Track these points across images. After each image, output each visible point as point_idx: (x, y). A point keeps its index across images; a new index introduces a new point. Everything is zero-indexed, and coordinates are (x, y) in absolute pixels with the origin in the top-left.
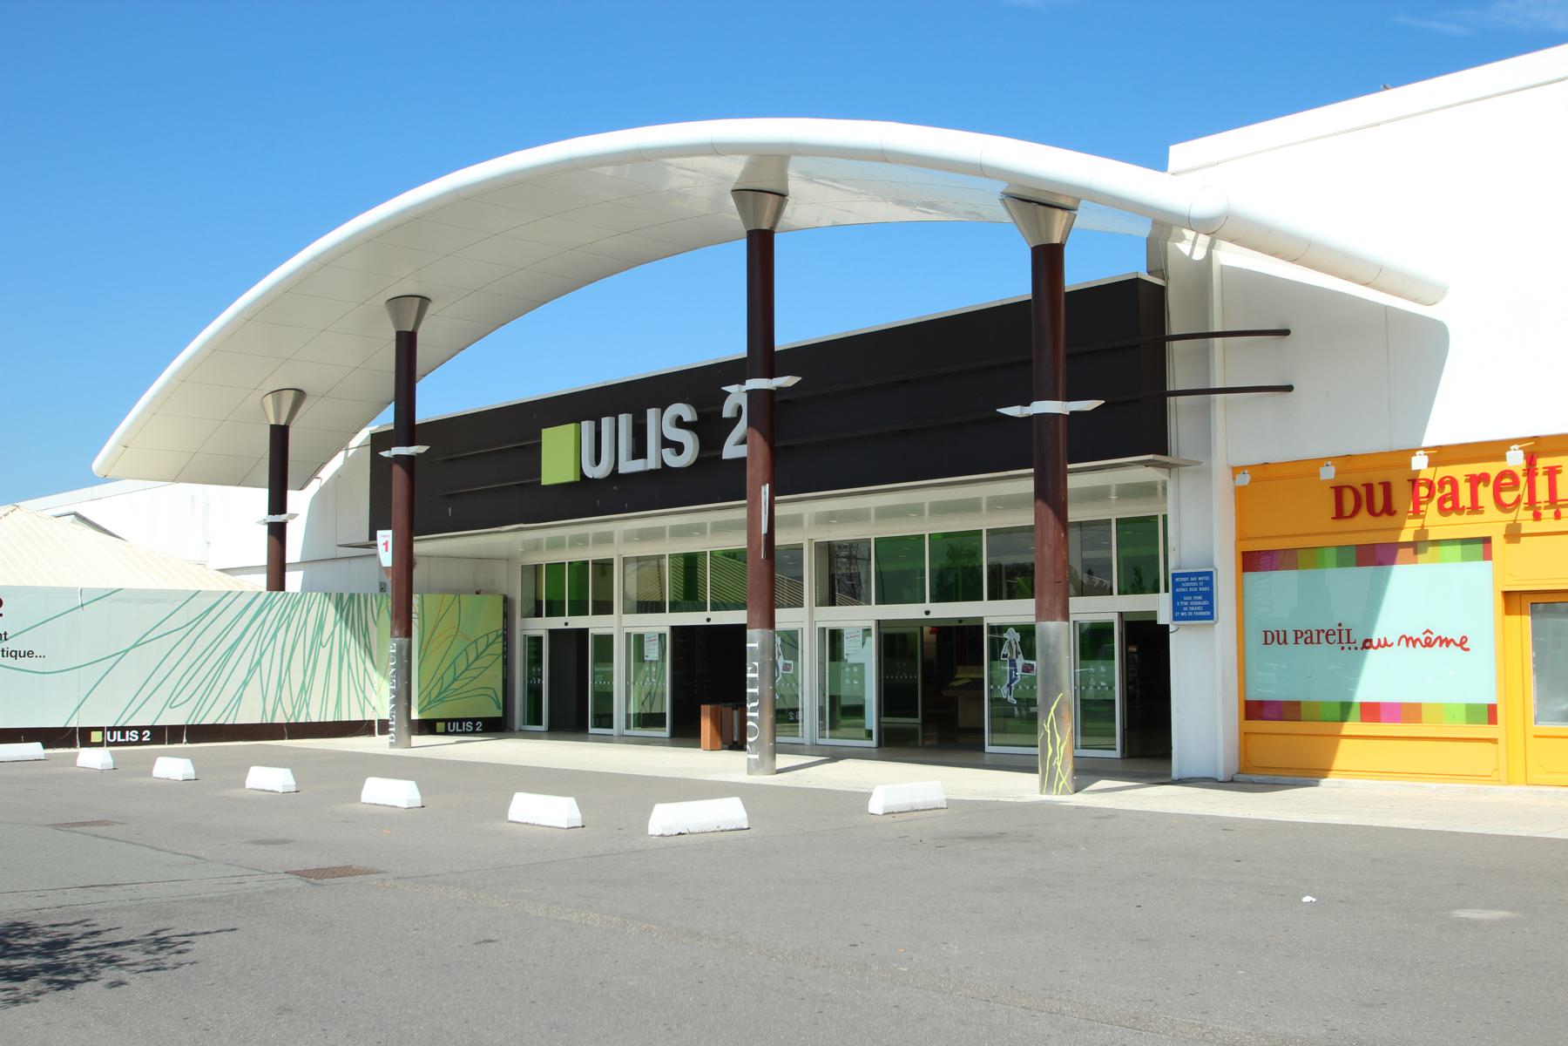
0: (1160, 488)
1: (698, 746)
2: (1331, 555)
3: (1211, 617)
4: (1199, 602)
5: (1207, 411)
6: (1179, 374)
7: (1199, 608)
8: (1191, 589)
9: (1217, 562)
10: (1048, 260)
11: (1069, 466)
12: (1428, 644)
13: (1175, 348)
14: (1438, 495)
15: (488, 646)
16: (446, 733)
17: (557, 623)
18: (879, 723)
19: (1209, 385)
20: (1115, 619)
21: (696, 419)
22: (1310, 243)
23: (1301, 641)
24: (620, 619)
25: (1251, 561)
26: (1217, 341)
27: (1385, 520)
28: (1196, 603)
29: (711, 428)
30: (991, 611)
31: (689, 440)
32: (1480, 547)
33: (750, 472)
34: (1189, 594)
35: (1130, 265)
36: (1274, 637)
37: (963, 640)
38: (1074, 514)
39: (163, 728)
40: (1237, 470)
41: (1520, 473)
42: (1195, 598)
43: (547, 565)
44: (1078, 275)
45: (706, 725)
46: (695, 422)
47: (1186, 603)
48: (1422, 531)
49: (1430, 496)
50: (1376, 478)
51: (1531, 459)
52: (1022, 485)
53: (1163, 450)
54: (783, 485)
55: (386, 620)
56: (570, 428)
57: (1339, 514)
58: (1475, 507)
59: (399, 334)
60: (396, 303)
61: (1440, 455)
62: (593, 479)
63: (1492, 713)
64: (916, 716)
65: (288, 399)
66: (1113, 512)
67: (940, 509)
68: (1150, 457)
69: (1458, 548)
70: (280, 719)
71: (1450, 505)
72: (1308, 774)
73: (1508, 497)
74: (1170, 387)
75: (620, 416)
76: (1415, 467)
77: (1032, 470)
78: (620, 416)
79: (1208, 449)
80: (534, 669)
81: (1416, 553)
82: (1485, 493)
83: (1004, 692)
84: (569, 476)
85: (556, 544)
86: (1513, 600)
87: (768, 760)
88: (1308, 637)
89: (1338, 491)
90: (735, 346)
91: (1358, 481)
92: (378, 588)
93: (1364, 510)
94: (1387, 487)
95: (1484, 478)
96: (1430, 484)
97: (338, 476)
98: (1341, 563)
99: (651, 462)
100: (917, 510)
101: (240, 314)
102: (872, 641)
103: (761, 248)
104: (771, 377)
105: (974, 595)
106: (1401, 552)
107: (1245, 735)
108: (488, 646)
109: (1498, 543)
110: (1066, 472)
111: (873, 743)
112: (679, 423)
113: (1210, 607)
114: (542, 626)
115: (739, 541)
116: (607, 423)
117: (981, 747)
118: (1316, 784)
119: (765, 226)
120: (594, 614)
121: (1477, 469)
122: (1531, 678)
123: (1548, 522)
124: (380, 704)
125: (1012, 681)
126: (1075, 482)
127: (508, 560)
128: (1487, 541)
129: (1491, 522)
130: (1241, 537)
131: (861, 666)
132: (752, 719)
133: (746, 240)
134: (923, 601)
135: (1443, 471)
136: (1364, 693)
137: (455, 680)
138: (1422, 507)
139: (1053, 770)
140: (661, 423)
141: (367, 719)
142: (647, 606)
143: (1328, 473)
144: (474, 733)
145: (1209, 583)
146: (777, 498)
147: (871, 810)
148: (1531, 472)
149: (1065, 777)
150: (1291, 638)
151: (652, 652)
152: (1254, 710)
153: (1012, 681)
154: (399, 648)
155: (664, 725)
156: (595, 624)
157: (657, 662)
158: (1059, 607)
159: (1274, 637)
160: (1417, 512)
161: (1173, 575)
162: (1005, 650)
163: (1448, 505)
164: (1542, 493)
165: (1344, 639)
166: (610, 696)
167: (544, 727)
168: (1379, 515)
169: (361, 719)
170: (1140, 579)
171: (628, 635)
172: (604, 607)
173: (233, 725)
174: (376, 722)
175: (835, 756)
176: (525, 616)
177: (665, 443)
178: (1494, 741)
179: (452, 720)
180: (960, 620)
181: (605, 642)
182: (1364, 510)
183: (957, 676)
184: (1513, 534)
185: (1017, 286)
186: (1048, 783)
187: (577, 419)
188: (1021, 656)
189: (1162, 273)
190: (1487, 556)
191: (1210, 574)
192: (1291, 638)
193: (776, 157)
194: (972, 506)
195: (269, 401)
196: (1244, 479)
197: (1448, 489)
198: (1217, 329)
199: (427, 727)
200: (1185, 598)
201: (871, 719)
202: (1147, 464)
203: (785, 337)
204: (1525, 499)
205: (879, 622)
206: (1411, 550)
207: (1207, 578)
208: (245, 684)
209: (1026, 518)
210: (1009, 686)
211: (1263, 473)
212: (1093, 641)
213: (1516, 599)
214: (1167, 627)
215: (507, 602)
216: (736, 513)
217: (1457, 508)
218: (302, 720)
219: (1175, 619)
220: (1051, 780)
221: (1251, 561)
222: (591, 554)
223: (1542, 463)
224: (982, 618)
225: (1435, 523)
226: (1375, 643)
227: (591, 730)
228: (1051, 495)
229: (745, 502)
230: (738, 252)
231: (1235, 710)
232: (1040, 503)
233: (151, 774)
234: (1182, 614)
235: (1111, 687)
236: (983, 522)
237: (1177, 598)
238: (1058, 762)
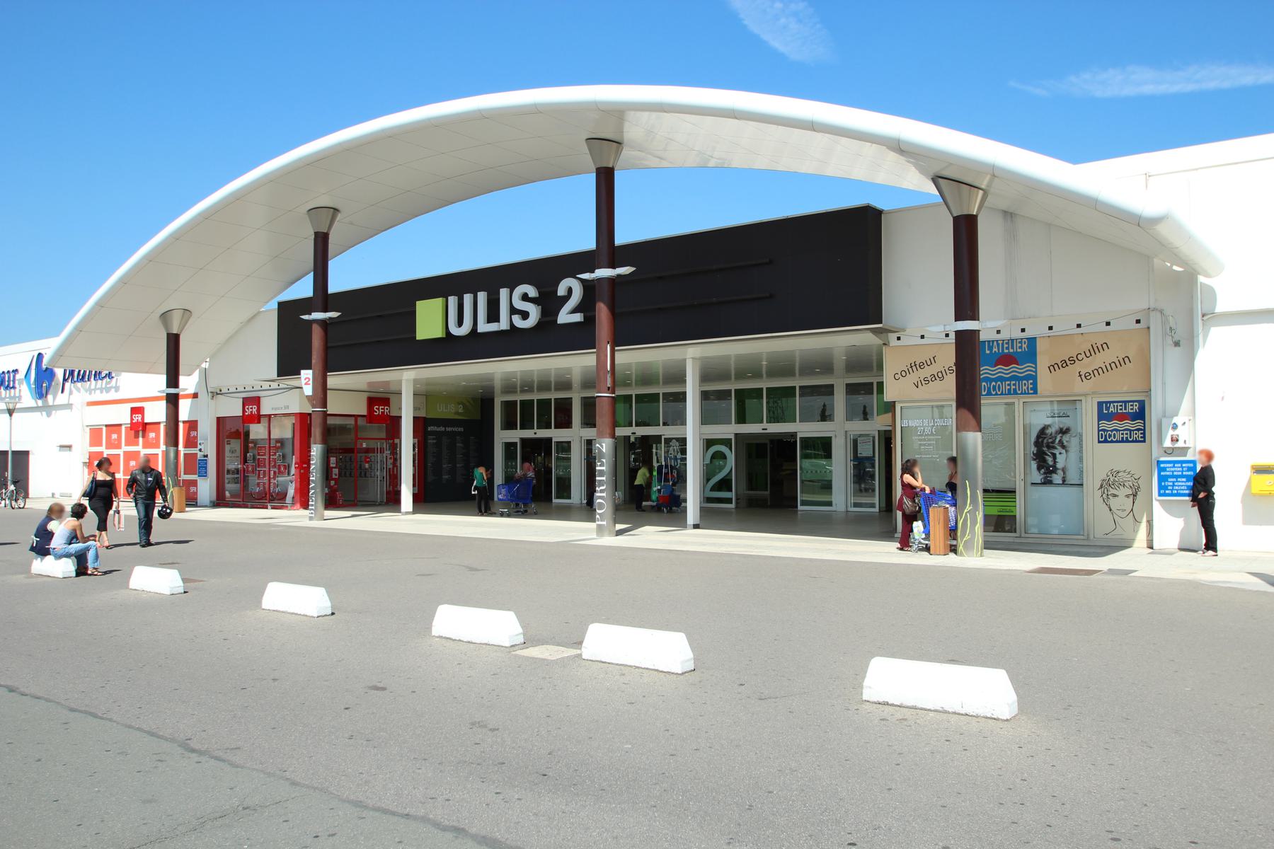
0: (875, 364)
7: (1183, 488)
8: (1175, 473)
17: (528, 434)
21: (538, 295)
28: (1180, 484)
29: (550, 303)
34: (1173, 476)
42: (1179, 479)
46: (537, 298)
47: (1171, 484)
56: (439, 302)
59: (316, 233)
64: (767, 490)
75: (449, 298)
78: (449, 298)
80: (510, 464)
84: (438, 333)
90: (586, 241)
99: (503, 325)
103: (605, 180)
112: (525, 297)
116: (468, 298)
133: (595, 174)
134: (762, 422)
145: (206, 464)
146: (616, 348)
156: (557, 435)
174: (519, 428)
177: (513, 311)
181: (565, 447)
183: (784, 468)
200: (1169, 480)
203: (624, 235)
207: (1192, 465)
229: (595, 350)
230: (590, 180)
234: (1167, 492)
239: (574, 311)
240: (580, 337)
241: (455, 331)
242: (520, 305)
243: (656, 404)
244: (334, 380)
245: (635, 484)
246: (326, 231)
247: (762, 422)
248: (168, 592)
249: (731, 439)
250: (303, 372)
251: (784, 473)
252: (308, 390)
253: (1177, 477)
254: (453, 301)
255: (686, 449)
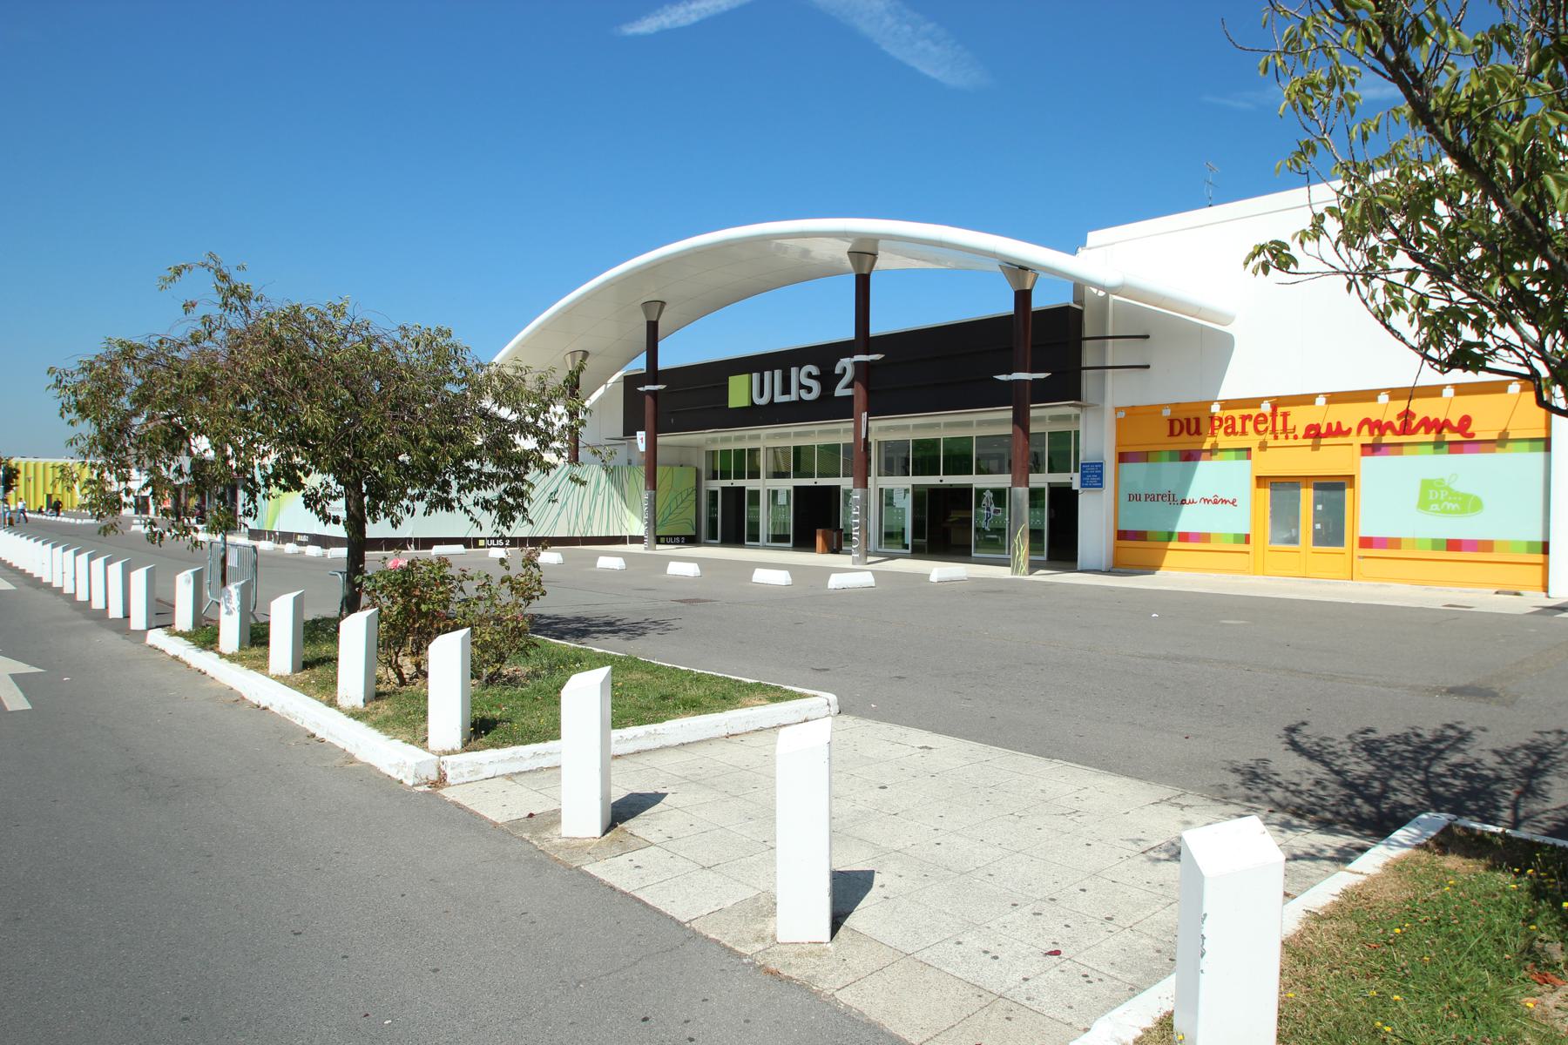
1: (815, 552)
2: (1166, 455)
3: (1101, 486)
4: (1095, 478)
5: (1103, 378)
6: (1089, 356)
9: (1105, 457)
10: (1023, 297)
11: (1031, 406)
12: (1216, 502)
13: (1087, 345)
14: (1224, 425)
15: (688, 495)
16: (666, 543)
17: (727, 483)
18: (913, 542)
19: (1104, 363)
20: (1046, 486)
21: (819, 374)
22: (1164, 298)
23: (1149, 500)
24: (764, 481)
25: (1123, 458)
26: (1110, 340)
27: (1195, 438)
29: (828, 379)
30: (976, 481)
31: (815, 385)
32: (1245, 453)
33: (856, 405)
34: (1089, 474)
35: (1064, 298)
36: (1134, 497)
37: (962, 496)
38: (1033, 429)
39: (516, 538)
40: (1117, 409)
41: (1268, 415)
43: (977, 437)
44: (1038, 303)
45: (819, 540)
48: (1215, 444)
49: (1220, 426)
50: (1192, 416)
51: (1274, 408)
52: (1007, 413)
53: (1078, 398)
54: (874, 411)
55: (642, 481)
56: (746, 377)
57: (1172, 434)
58: (1244, 432)
59: (648, 322)
60: (646, 305)
61: (1226, 405)
62: (759, 405)
63: (1247, 539)
65: (579, 356)
66: (1046, 428)
67: (949, 425)
68: (1073, 402)
69: (1233, 453)
70: (577, 534)
71: (1231, 431)
72: (1150, 568)
73: (1261, 427)
74: (1083, 365)
76: (1213, 411)
77: (1011, 407)
79: (1102, 397)
81: (1211, 455)
82: (1249, 425)
83: (983, 524)
84: (745, 403)
85: (727, 440)
86: (1261, 481)
87: (863, 559)
88: (1152, 498)
89: (1172, 422)
90: (848, 333)
91: (1182, 416)
92: (627, 462)
93: (1185, 432)
94: (1198, 420)
95: (1249, 417)
96: (1220, 420)
97: (601, 399)
98: (1172, 459)
99: (793, 397)
100: (906, 427)
101: (560, 310)
102: (910, 496)
103: (863, 284)
104: (868, 354)
105: (967, 471)
106: (1204, 454)
107: (1117, 548)
108: (688, 495)
109: (1255, 451)
110: (1029, 408)
111: (909, 551)
112: (810, 375)
113: (1101, 481)
114: (718, 485)
115: (850, 439)
116: (767, 374)
117: (971, 554)
118: (1153, 573)
119: (865, 272)
120: (748, 478)
121: (1246, 412)
122: (1268, 521)
123: (1282, 441)
124: (637, 527)
125: (988, 518)
126: (1033, 413)
127: (698, 447)
128: (1249, 450)
129: (1252, 440)
130: (1118, 445)
131: (903, 509)
132: (855, 536)
135: (1228, 413)
136: (1182, 526)
137: (670, 514)
138: (1216, 431)
139: (1019, 563)
140: (799, 375)
141: (623, 535)
142: (778, 475)
143: (1167, 413)
144: (680, 544)
145: (1101, 469)
147: (931, 580)
148: (1274, 415)
149: (1025, 567)
150: (1143, 498)
151: (782, 500)
152: (1122, 535)
153: (988, 518)
154: (650, 497)
155: (789, 541)
156: (749, 484)
157: (784, 505)
158: (1024, 480)
159: (1134, 497)
160: (1213, 434)
161: (1082, 464)
162: (984, 502)
163: (1229, 430)
164: (1279, 426)
165: (1171, 499)
166: (757, 524)
167: (719, 540)
168: (1193, 435)
169: (619, 535)
170: (1060, 462)
171: (769, 490)
172: (755, 474)
173: (553, 537)
174: (1072, 470)
175: (892, 557)
176: (707, 479)
177: (801, 386)
178: (1248, 553)
179: (668, 536)
180: (951, 485)
181: (755, 495)
182: (1185, 432)
184: (1263, 446)
185: (1007, 307)
186: (1015, 571)
187: (750, 372)
188: (993, 505)
189: (1081, 302)
190: (1249, 457)
191: (1102, 463)
192: (1143, 498)
193: (874, 239)
194: (968, 424)
195: (569, 358)
196: (1122, 415)
197: (1230, 422)
198: (1110, 335)
199: (658, 541)
201: (908, 539)
202: (1070, 405)
203: (876, 329)
204: (1270, 429)
205: (913, 485)
206: (1209, 454)
208: (559, 515)
209: (1008, 430)
210: (986, 521)
211: (1131, 411)
212: (1035, 494)
213: (1263, 480)
214: (1077, 491)
215: (698, 472)
216: (847, 425)
217: (1234, 433)
218: (589, 535)
219: (1082, 487)
220: (1017, 568)
221: (1123, 458)
222: (747, 445)
223: (1280, 410)
224: (972, 484)
225: (1222, 440)
226: (1187, 502)
227: (746, 543)
228: (1021, 420)
231: (1112, 535)
232: (1015, 426)
233: (751, 579)
235: (1043, 523)
236: (974, 433)
237: (1083, 476)
238: (1021, 559)
239: (847, 387)
240: (842, 409)
241: (758, 401)
242: (806, 382)
243: (1295, 491)
244: (662, 439)
245: (30, 707)
246: (655, 320)
247: (939, 475)
248: (693, 575)
249: (717, 491)
250: (638, 433)
251: (951, 520)
252: (642, 447)
253: (1093, 474)
254: (756, 376)
255: (421, 539)
